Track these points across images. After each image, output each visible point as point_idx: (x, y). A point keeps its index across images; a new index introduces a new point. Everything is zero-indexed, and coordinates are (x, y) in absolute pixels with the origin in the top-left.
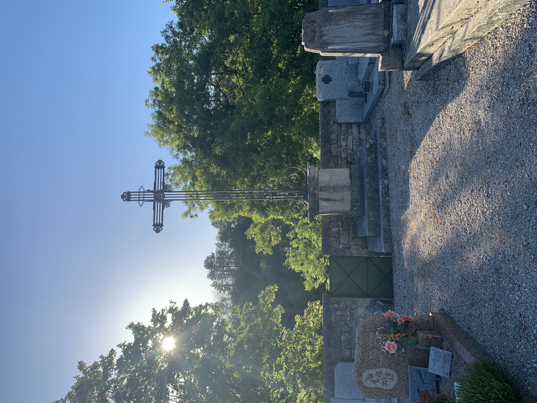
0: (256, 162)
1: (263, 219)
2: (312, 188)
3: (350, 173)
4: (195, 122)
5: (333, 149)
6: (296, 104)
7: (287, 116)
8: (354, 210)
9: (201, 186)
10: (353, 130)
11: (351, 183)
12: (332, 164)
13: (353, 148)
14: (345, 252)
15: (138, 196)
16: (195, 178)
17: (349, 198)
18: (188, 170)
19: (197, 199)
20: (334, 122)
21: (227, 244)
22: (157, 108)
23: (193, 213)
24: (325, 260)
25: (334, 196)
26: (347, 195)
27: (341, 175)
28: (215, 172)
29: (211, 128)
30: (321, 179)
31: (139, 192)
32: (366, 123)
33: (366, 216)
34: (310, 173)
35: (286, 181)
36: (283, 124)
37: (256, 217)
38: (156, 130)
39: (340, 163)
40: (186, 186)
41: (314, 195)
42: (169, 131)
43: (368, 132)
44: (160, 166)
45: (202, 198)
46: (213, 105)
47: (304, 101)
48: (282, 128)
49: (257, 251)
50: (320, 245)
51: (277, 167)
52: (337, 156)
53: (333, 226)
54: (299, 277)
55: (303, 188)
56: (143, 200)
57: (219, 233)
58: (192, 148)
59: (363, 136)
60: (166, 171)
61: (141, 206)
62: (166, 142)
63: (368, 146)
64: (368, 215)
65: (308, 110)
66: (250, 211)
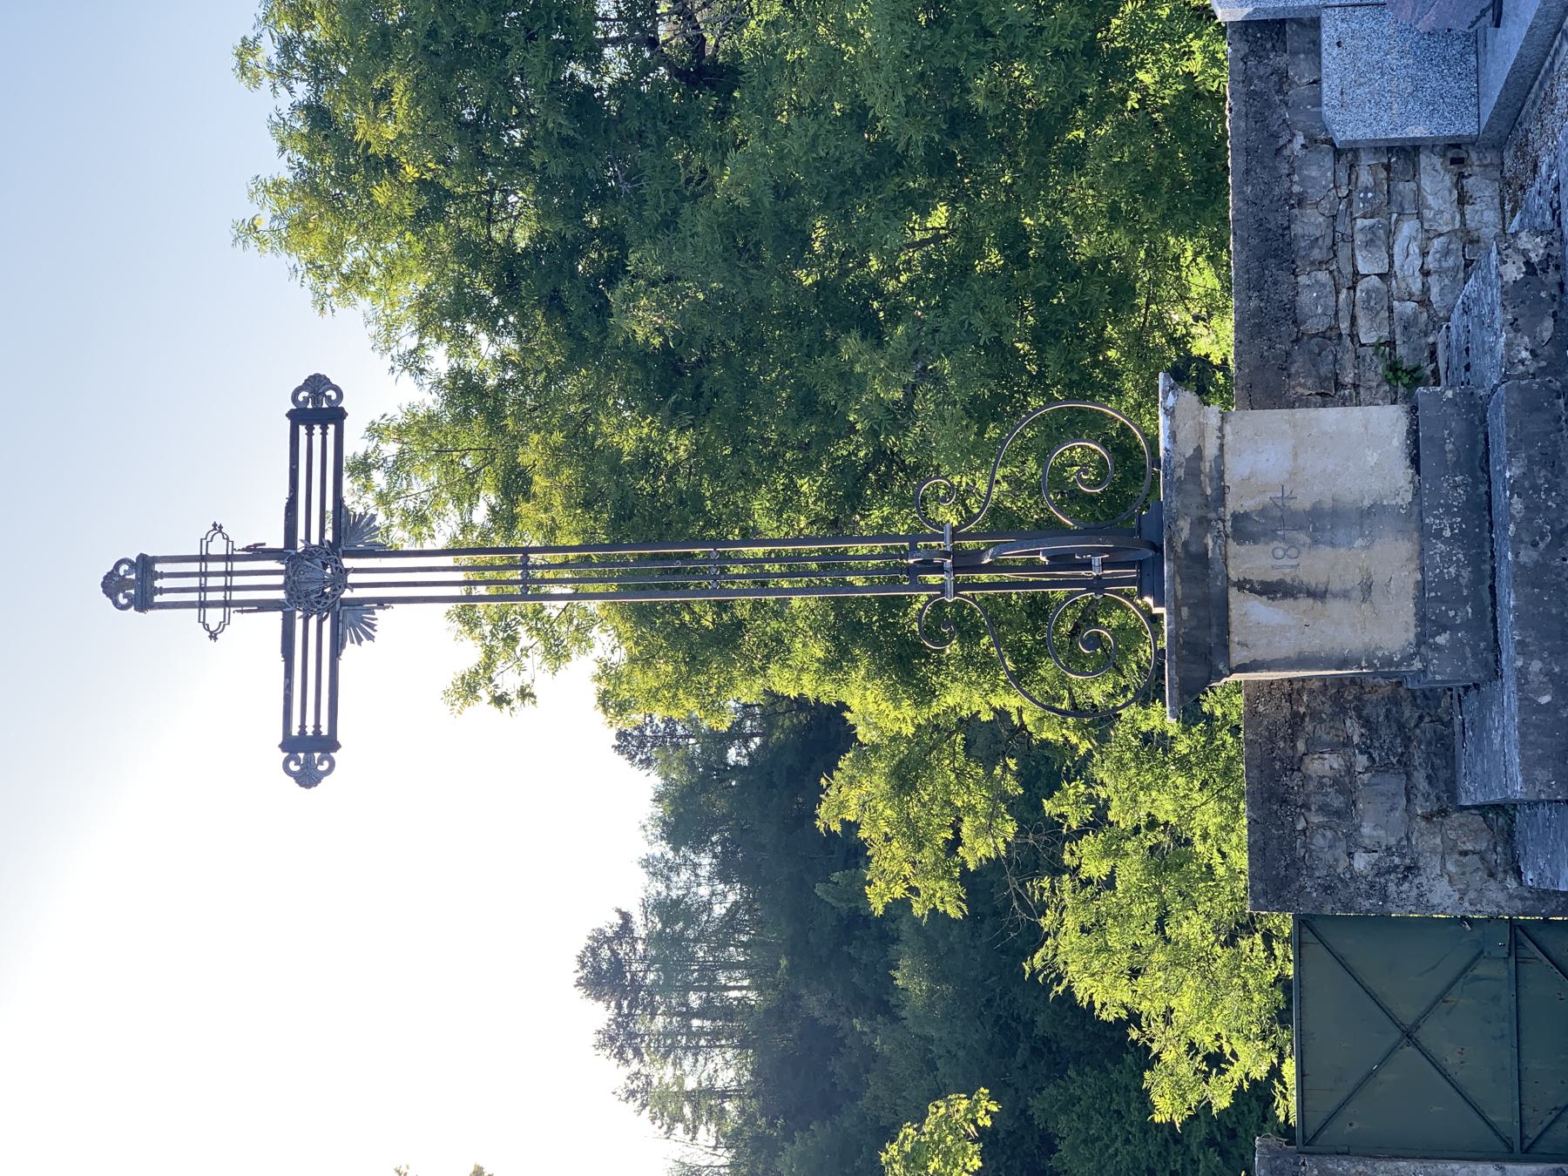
0: (861, 383)
1: (907, 709)
2: (1185, 525)
4: (518, 160)
5: (1306, 298)
6: (1091, 50)
7: (1037, 117)
8: (1437, 648)
9: (552, 517)
10: (1426, 183)
11: (1417, 493)
12: (1303, 386)
13: (1426, 290)
14: (1385, 898)
15: (194, 582)
16: (515, 485)
17: (1407, 578)
18: (477, 433)
19: (523, 597)
20: (1311, 142)
21: (706, 861)
22: (302, 90)
23: (508, 681)
24: (1269, 948)
25: (1314, 565)
26: (1393, 561)
27: (1357, 447)
28: (628, 446)
29: (602, 198)
30: (1235, 470)
31: (204, 558)
32: (1499, 146)
33: (1510, 685)
34: (1173, 436)
35: (1036, 490)
36: (1015, 167)
37: (873, 707)
38: (295, 213)
39: (1348, 379)
40: (467, 527)
41: (1198, 563)
42: (376, 223)
43: (1511, 195)
44: (317, 408)
45: (556, 590)
46: (616, 63)
47: (1136, 29)
48: (1008, 189)
49: (877, 899)
50: (1241, 860)
51: (981, 412)
52: (1330, 335)
53: (1313, 746)
54: (1117, 1049)
55: (1133, 518)
56: (226, 604)
57: (659, 798)
58: (498, 313)
59: (1483, 216)
60: (356, 444)
61: (213, 636)
62: (356, 279)
63: (1513, 272)
64: (1522, 673)
65: (1163, 81)
66: (833, 665)
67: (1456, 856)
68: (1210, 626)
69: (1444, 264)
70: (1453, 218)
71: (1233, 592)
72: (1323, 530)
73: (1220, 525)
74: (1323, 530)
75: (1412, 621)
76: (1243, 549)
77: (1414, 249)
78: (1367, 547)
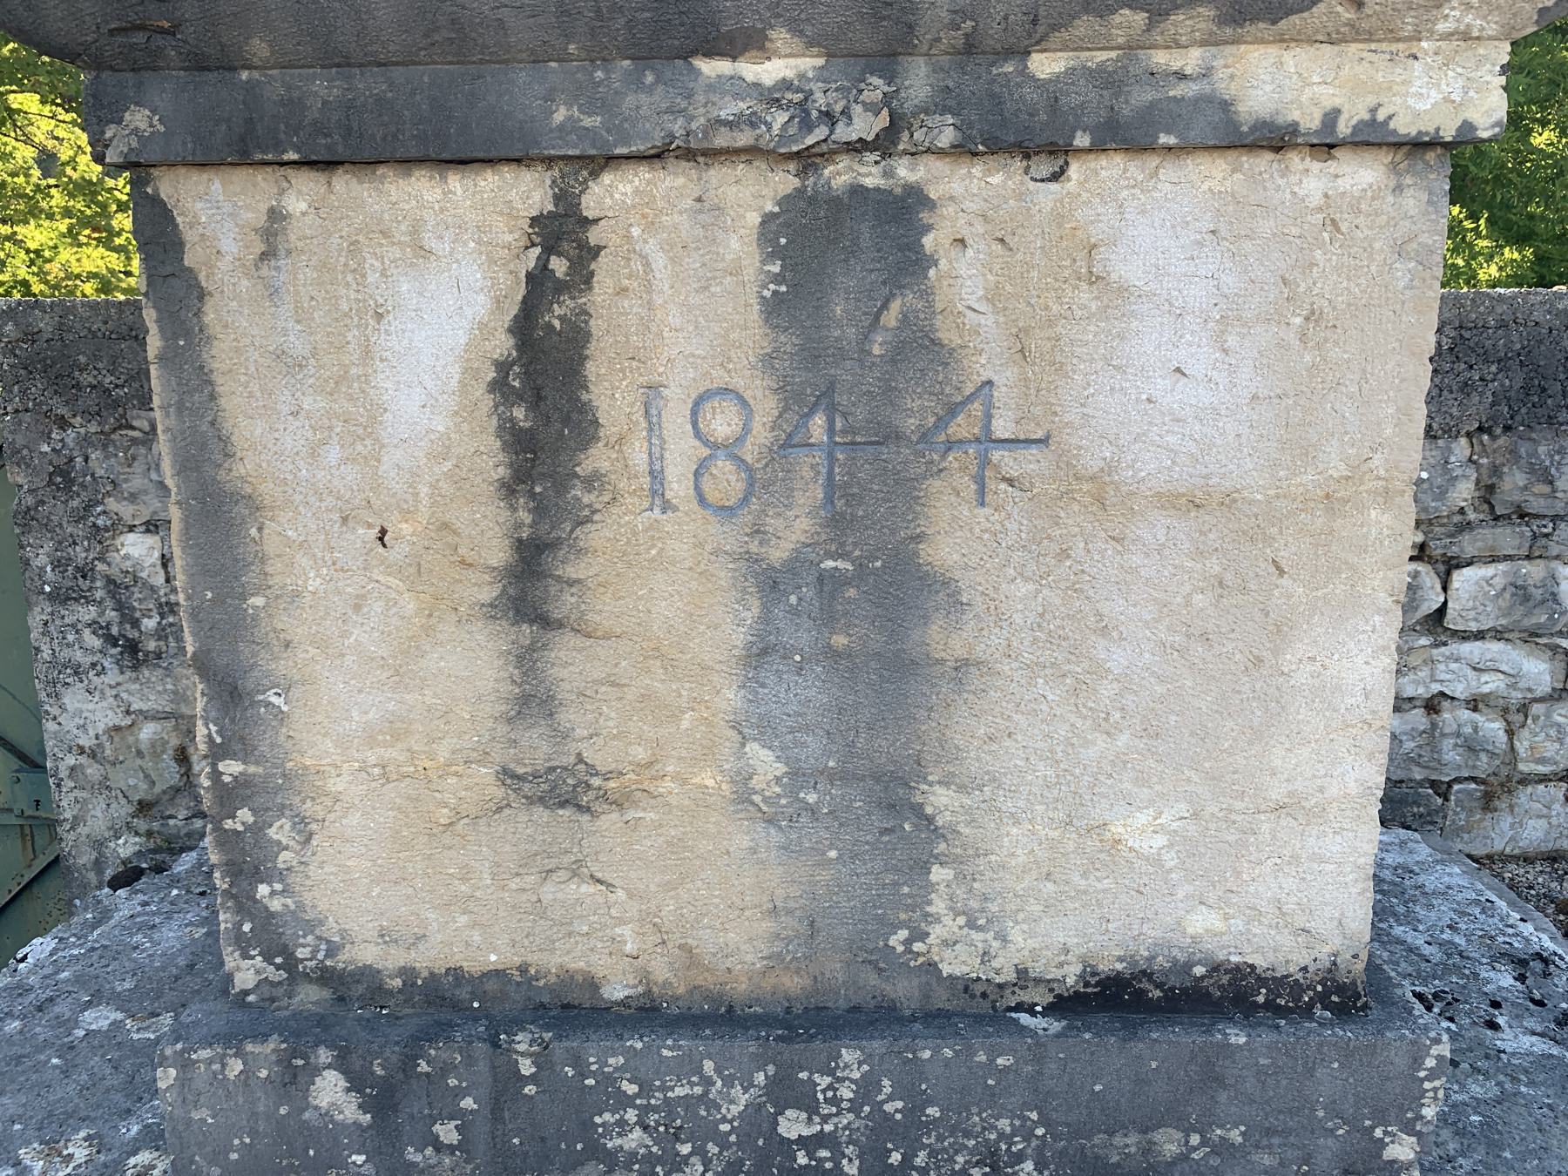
3: (1226, 995)
11: (982, 1008)
14: (61, 597)
25: (670, 581)
26: (687, 884)
30: (1150, 219)
67: (175, 742)
68: (339, 61)
69: (1448, 743)
70: (1542, 761)
71: (528, 192)
72: (828, 619)
73: (864, 125)
74: (828, 619)
75: (429, 957)
76: (740, 245)
77: (1491, 684)
78: (743, 795)
